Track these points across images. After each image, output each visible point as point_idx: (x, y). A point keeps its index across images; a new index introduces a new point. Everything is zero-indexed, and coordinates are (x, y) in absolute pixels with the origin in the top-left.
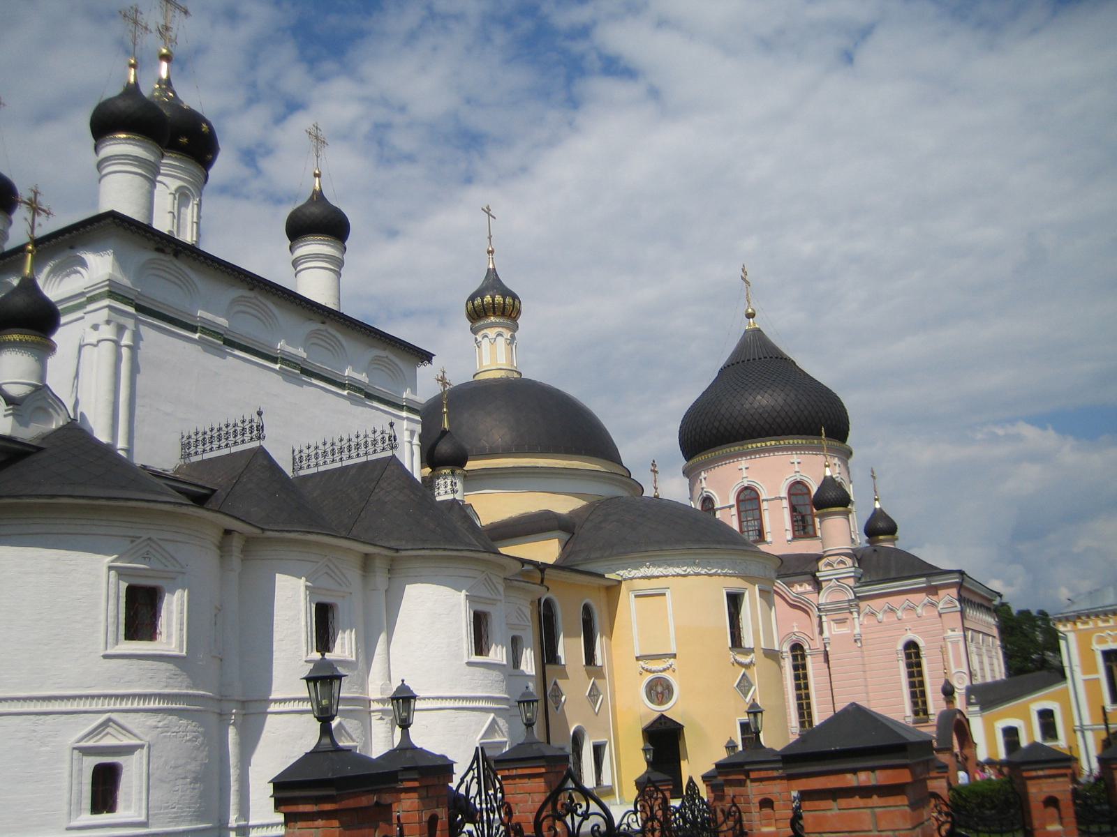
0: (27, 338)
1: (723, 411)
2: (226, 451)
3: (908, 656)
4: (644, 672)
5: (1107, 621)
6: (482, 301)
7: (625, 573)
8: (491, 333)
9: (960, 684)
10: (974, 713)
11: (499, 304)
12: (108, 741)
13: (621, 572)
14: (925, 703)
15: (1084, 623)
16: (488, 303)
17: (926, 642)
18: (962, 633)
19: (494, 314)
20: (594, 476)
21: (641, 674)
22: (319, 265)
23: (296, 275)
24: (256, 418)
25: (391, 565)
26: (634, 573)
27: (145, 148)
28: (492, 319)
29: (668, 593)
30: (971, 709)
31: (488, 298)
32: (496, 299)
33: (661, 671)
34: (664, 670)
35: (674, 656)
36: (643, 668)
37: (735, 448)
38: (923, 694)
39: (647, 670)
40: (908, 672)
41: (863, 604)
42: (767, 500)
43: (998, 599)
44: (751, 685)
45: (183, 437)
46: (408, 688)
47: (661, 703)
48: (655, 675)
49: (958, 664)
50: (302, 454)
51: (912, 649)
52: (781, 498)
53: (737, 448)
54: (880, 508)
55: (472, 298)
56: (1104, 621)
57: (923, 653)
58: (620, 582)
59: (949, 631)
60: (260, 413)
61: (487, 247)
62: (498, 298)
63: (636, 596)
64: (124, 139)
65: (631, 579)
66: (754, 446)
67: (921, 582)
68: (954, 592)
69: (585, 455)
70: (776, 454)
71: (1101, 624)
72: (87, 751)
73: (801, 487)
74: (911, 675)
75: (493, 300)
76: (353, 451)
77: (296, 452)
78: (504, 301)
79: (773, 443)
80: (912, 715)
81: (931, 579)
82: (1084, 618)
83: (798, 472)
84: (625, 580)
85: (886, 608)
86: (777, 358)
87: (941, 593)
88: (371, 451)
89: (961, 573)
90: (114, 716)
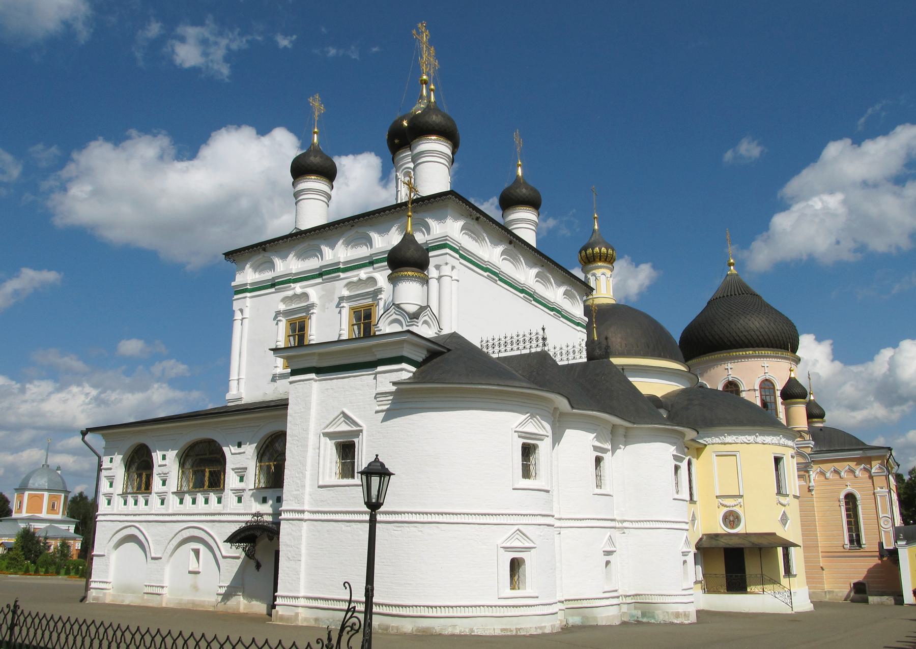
0: (416, 274)
2: (518, 353)
3: (847, 503)
4: (721, 506)
6: (593, 251)
7: (709, 440)
8: (598, 272)
9: (885, 525)
10: (901, 546)
11: (604, 253)
12: (517, 544)
13: (707, 439)
16: (590, 254)
20: (674, 373)
21: (719, 508)
22: (322, 199)
23: (296, 203)
24: (541, 332)
25: (626, 432)
26: (716, 440)
28: (600, 264)
30: (899, 543)
32: (602, 250)
33: (733, 507)
36: (721, 504)
37: (724, 354)
39: (723, 505)
40: (847, 514)
43: (896, 467)
45: (482, 342)
46: (382, 465)
47: (733, 528)
48: (728, 509)
50: (488, 343)
53: (725, 355)
54: (814, 400)
57: (859, 503)
58: (706, 445)
59: (878, 488)
60: (543, 329)
62: (604, 250)
63: (716, 456)
64: (434, 140)
65: (713, 444)
66: (738, 353)
67: (858, 454)
69: (669, 358)
70: (750, 360)
72: (506, 549)
73: (769, 383)
75: (600, 251)
76: (577, 354)
78: (607, 252)
79: (751, 352)
80: (849, 544)
83: (767, 373)
84: (709, 444)
85: (833, 469)
86: (751, 294)
88: (578, 357)
90: (520, 527)
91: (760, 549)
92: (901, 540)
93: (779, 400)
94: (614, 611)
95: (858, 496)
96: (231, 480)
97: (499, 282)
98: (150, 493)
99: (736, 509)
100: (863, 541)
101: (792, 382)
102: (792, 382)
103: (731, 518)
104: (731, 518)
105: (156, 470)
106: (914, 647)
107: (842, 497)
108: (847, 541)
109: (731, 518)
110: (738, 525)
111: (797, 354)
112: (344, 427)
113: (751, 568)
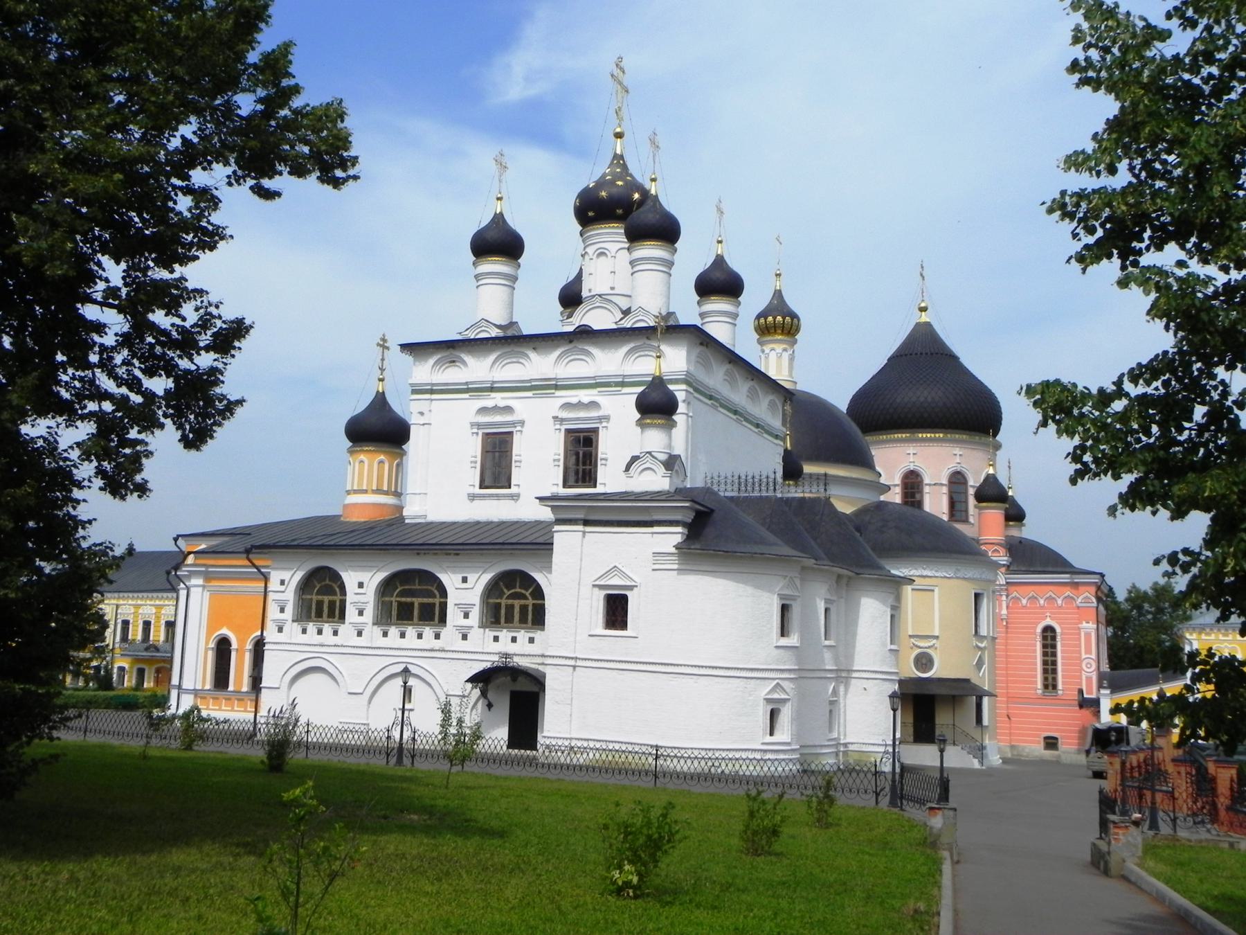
1: (898, 401)
3: (1044, 638)
5: (1227, 635)
10: (1105, 695)
12: (776, 696)
14: (1055, 679)
15: (1207, 634)
17: (1062, 628)
18: (1095, 626)
19: (783, 333)
27: (660, 247)
28: (780, 337)
29: (936, 590)
30: (1103, 691)
31: (770, 319)
34: (929, 647)
35: (937, 637)
38: (1054, 671)
41: (1011, 588)
42: (930, 485)
44: (983, 664)
49: (1088, 651)
51: (1049, 633)
52: (942, 485)
55: (758, 317)
56: (1224, 635)
57: (1059, 638)
61: (716, 238)
67: (1065, 578)
68: (1093, 589)
71: (1221, 637)
74: (1045, 654)
77: (749, 477)
79: (941, 435)
81: (1074, 576)
82: (1208, 630)
87: (1082, 588)
89: (1102, 575)
91: (954, 697)
92: (1104, 688)
93: (972, 501)
94: (832, 761)
95: (1058, 630)
96: (453, 615)
97: (744, 423)
98: (344, 623)
99: (928, 651)
100: (1060, 686)
101: (991, 480)
102: (991, 480)
103: (924, 661)
104: (924, 661)
105: (350, 598)
106: (1244, 612)
107: (1039, 630)
108: (1040, 685)
109: (924, 661)
110: (931, 669)
111: (997, 438)
112: (616, 581)
113: (943, 719)
